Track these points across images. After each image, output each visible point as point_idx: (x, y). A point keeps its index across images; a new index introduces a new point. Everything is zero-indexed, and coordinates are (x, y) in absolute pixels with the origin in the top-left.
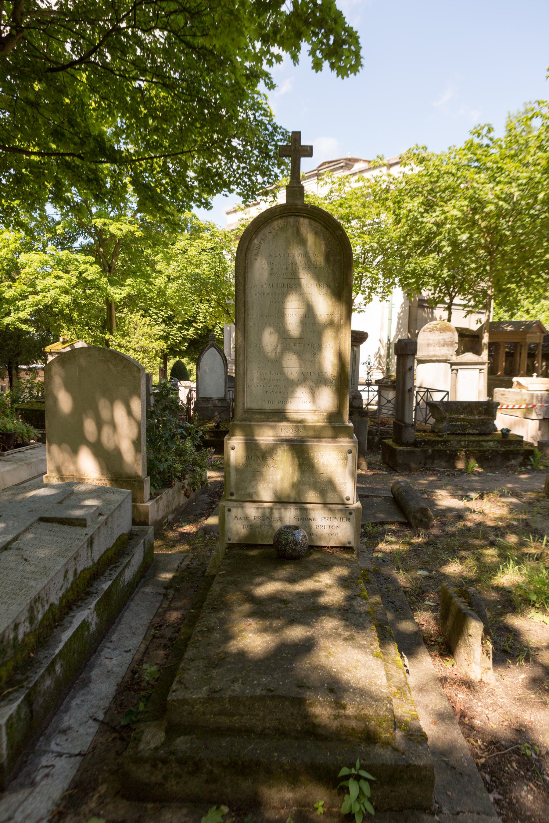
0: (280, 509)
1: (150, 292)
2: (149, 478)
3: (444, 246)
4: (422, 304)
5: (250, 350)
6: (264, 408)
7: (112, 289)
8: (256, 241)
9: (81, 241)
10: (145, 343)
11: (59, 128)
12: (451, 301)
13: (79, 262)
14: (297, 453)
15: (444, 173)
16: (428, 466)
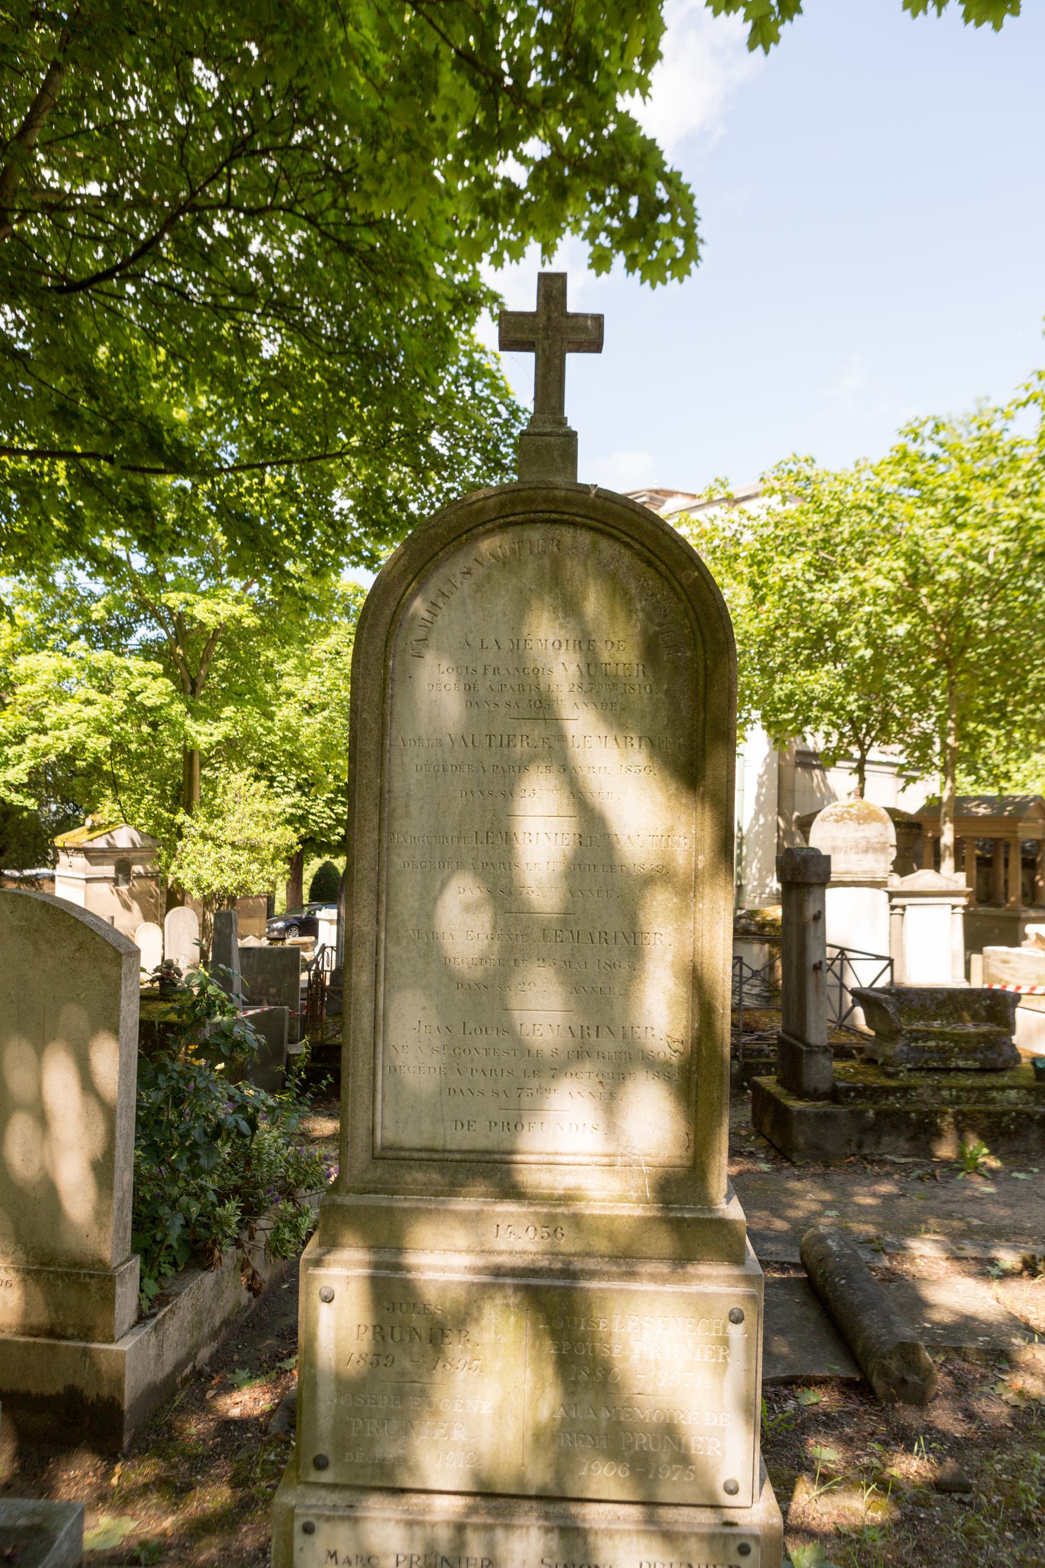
0: (489, 1528)
1: (269, 734)
2: (136, 1262)
3: (857, 648)
4: (807, 760)
5: (393, 950)
6: (439, 1144)
7: (194, 725)
8: (419, 606)
9: (145, 632)
10: (254, 832)
11: (68, 404)
12: (863, 756)
13: (130, 673)
14: (549, 1320)
15: (853, 507)
16: (866, 1151)
